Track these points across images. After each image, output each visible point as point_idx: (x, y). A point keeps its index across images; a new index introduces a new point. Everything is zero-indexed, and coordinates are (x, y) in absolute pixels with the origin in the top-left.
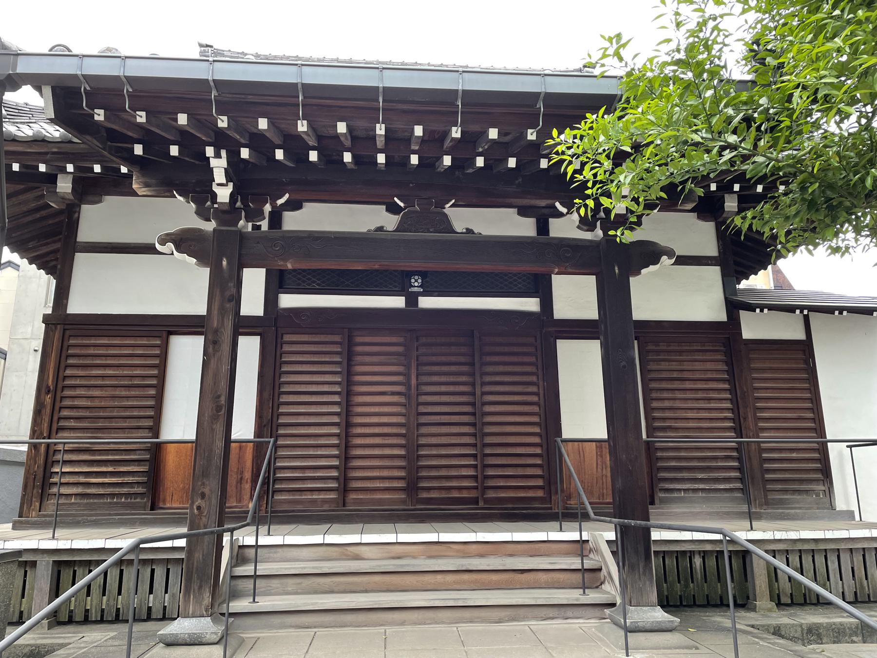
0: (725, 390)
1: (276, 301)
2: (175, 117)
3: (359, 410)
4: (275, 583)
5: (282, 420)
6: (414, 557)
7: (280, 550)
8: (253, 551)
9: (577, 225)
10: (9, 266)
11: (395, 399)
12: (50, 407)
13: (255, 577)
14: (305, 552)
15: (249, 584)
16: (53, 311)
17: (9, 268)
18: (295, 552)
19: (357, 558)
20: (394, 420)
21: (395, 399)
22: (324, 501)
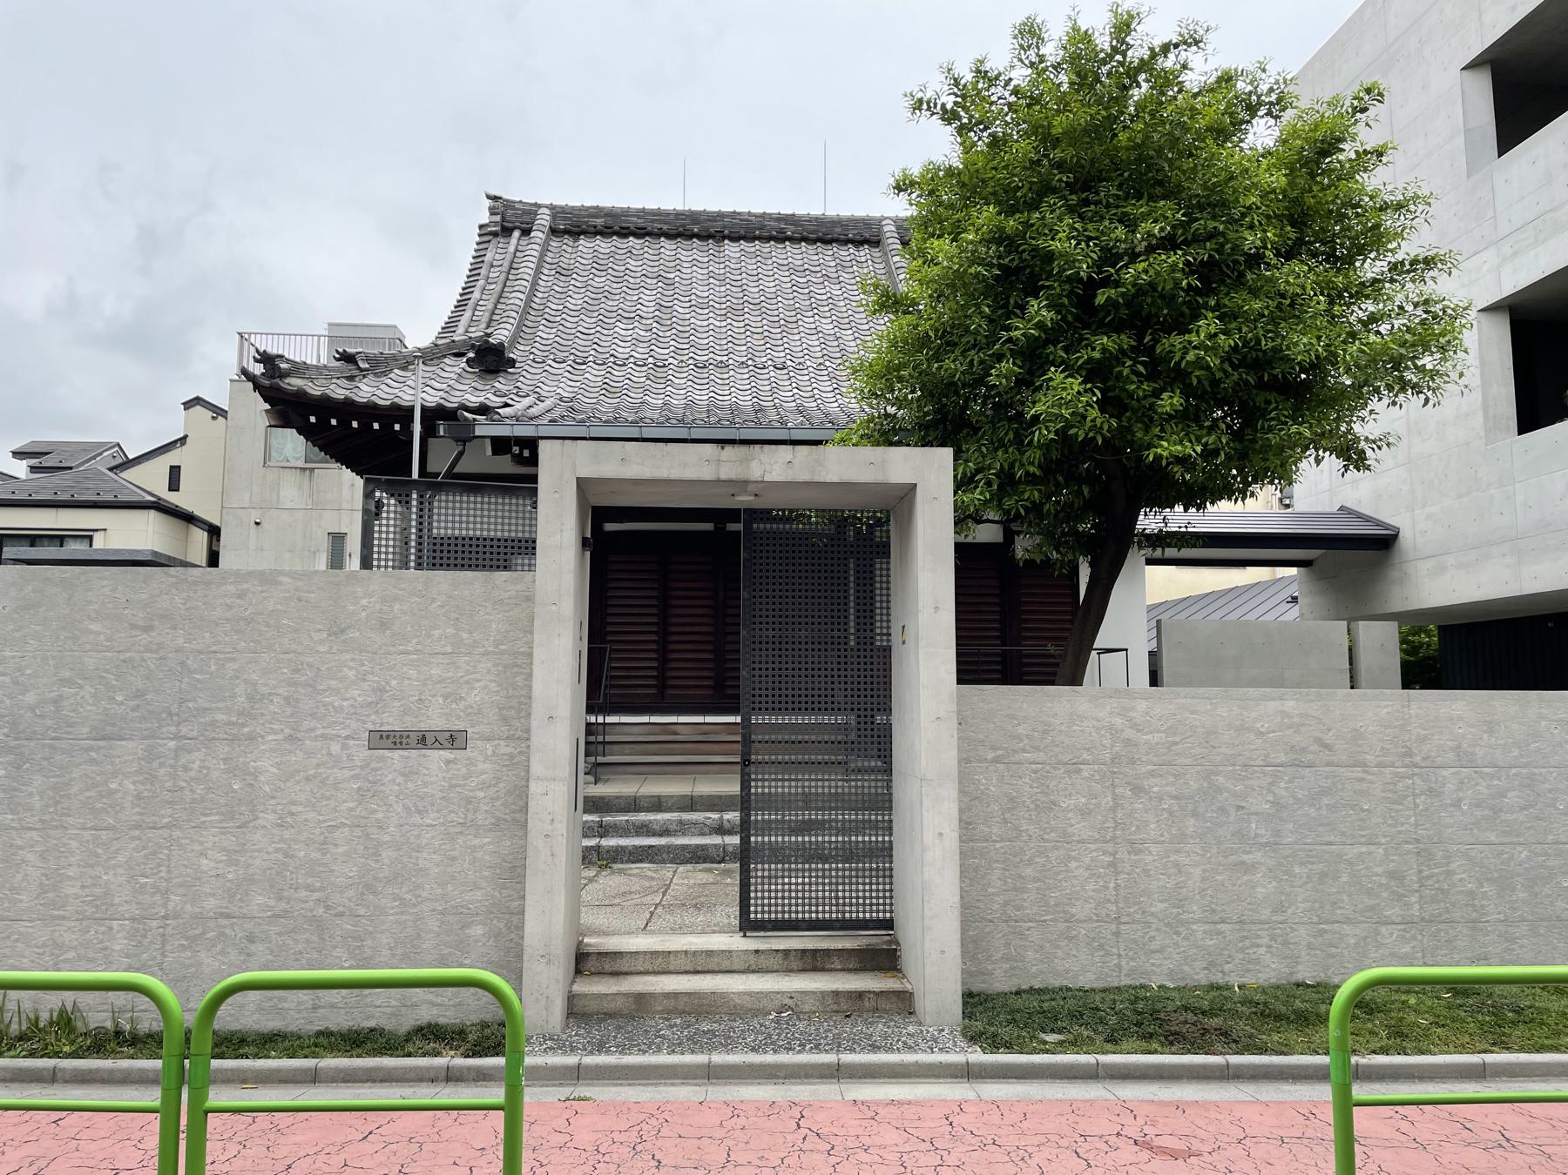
0: (996, 621)
1: (601, 527)
2: (737, 675)
3: (674, 620)
4: (616, 747)
5: (609, 629)
6: (717, 734)
7: (617, 727)
8: (602, 727)
9: (520, 192)
10: (198, 404)
11: (704, 611)
12: (360, 1088)
13: (604, 743)
14: (636, 729)
15: (600, 748)
16: (162, 1103)
17: (198, 407)
18: (627, 729)
19: (675, 733)
20: (704, 629)
21: (704, 611)
22: (647, 695)
